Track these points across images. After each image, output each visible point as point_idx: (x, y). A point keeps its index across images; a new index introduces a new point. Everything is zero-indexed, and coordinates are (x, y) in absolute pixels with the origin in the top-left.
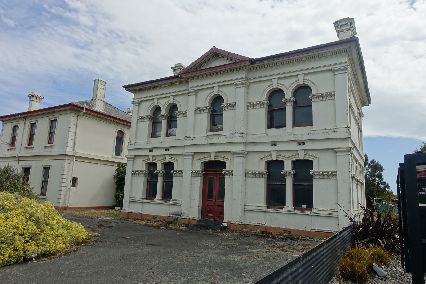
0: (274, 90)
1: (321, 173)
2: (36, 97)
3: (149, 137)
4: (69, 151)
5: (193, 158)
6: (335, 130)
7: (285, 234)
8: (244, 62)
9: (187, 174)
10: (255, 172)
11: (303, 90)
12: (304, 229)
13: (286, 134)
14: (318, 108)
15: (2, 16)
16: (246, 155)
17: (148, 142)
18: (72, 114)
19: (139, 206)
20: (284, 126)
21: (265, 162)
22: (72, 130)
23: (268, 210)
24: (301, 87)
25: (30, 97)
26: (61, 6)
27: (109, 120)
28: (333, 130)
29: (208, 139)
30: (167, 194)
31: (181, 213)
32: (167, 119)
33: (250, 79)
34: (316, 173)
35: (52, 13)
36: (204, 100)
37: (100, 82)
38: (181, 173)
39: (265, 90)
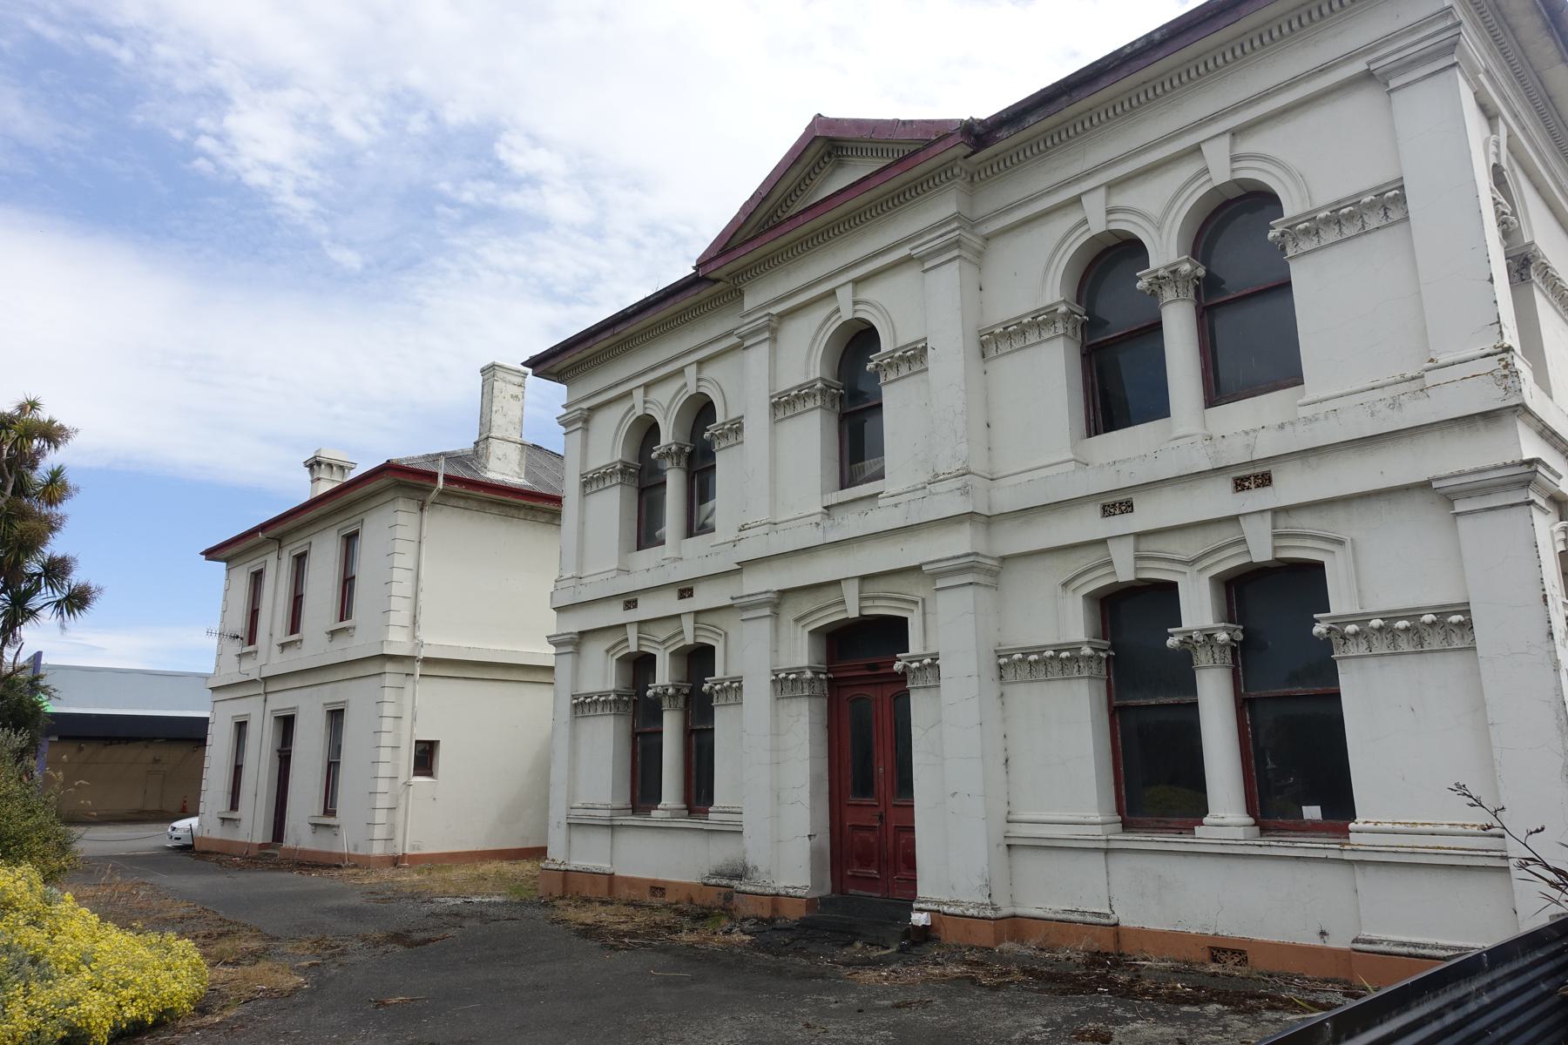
0: (1099, 248)
1: (1376, 623)
2: (330, 466)
3: (624, 551)
4: (398, 641)
5: (776, 615)
6: (1430, 379)
7: (1213, 968)
8: (940, 147)
9: (758, 690)
10: (1040, 650)
11: (1237, 212)
12: (1318, 942)
13: (1174, 444)
14: (1328, 296)
15: (325, 243)
16: (994, 573)
17: (624, 571)
18: (401, 504)
19: (600, 840)
20: (1160, 410)
21: (1089, 597)
22: (404, 561)
23: (1138, 840)
24: (1228, 203)
25: (311, 466)
26: (489, 177)
27: (544, 511)
28: (1414, 385)
29: (828, 523)
30: (699, 791)
31: (745, 868)
32: (683, 463)
33: (986, 220)
34: (1351, 628)
35: (464, 205)
36: (803, 355)
37: (500, 374)
38: (735, 688)
39: (1054, 254)
